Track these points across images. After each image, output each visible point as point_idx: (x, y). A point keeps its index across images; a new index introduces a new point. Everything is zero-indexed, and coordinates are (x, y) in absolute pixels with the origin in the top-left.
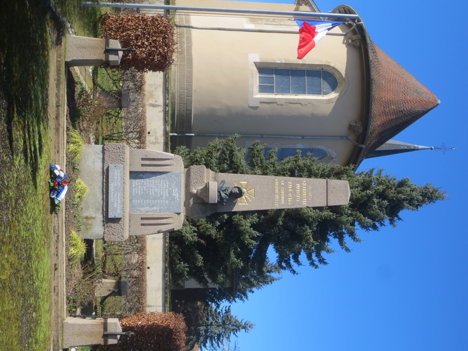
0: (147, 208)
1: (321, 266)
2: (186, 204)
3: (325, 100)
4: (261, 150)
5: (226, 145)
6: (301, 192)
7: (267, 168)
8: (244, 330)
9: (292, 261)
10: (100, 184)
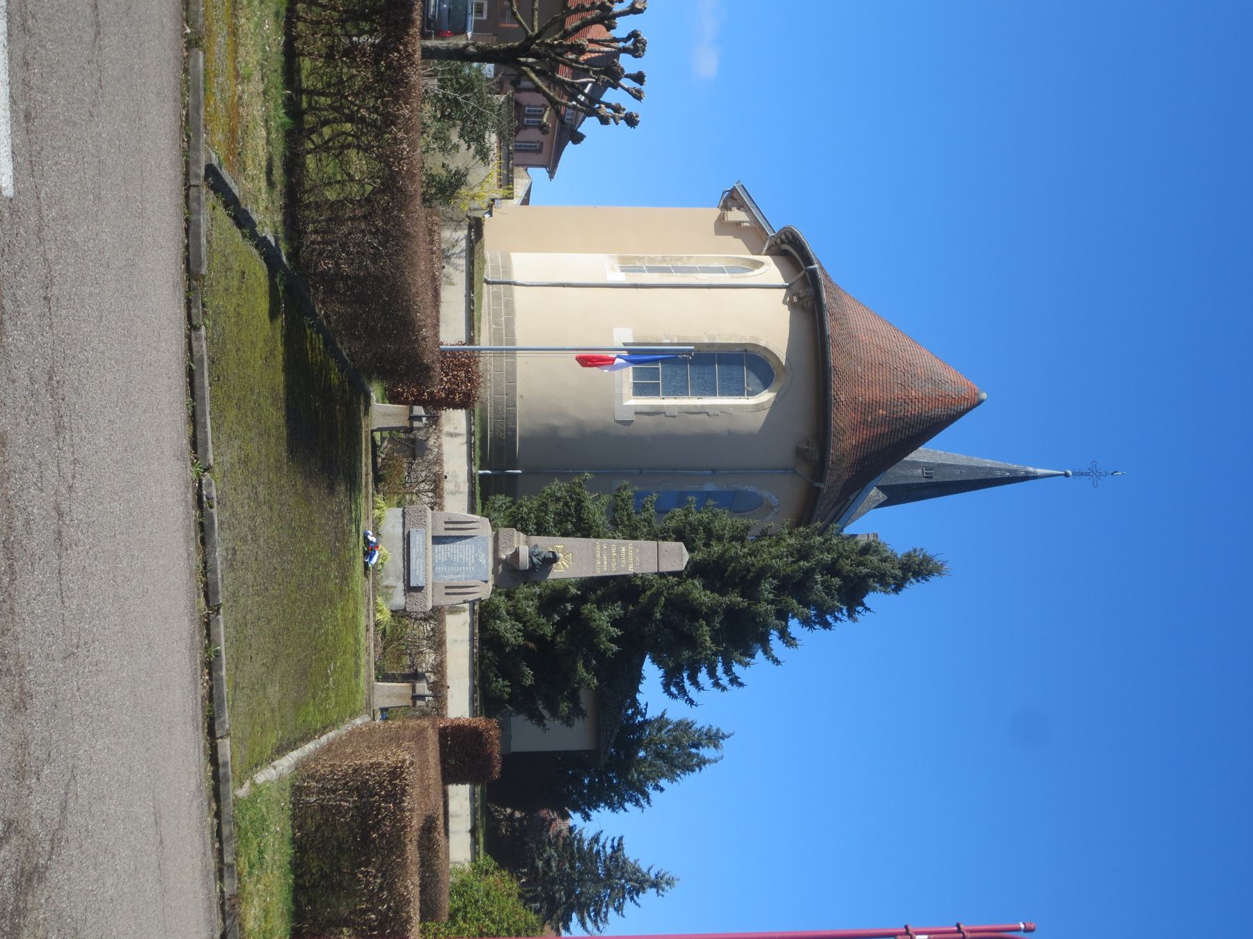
0: (451, 576)
1: (734, 689)
2: (495, 571)
3: (757, 402)
4: (629, 498)
5: (570, 491)
6: (627, 556)
7: (636, 528)
8: (654, 890)
9: (687, 683)
10: (401, 550)
